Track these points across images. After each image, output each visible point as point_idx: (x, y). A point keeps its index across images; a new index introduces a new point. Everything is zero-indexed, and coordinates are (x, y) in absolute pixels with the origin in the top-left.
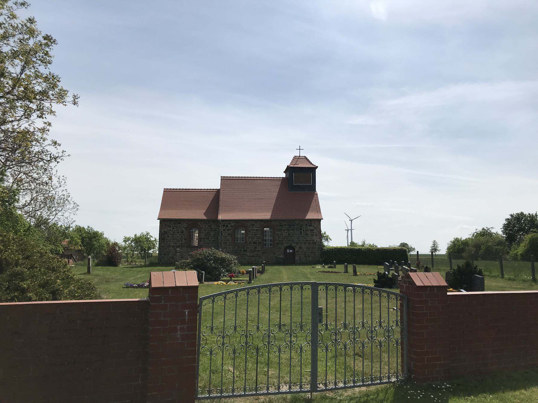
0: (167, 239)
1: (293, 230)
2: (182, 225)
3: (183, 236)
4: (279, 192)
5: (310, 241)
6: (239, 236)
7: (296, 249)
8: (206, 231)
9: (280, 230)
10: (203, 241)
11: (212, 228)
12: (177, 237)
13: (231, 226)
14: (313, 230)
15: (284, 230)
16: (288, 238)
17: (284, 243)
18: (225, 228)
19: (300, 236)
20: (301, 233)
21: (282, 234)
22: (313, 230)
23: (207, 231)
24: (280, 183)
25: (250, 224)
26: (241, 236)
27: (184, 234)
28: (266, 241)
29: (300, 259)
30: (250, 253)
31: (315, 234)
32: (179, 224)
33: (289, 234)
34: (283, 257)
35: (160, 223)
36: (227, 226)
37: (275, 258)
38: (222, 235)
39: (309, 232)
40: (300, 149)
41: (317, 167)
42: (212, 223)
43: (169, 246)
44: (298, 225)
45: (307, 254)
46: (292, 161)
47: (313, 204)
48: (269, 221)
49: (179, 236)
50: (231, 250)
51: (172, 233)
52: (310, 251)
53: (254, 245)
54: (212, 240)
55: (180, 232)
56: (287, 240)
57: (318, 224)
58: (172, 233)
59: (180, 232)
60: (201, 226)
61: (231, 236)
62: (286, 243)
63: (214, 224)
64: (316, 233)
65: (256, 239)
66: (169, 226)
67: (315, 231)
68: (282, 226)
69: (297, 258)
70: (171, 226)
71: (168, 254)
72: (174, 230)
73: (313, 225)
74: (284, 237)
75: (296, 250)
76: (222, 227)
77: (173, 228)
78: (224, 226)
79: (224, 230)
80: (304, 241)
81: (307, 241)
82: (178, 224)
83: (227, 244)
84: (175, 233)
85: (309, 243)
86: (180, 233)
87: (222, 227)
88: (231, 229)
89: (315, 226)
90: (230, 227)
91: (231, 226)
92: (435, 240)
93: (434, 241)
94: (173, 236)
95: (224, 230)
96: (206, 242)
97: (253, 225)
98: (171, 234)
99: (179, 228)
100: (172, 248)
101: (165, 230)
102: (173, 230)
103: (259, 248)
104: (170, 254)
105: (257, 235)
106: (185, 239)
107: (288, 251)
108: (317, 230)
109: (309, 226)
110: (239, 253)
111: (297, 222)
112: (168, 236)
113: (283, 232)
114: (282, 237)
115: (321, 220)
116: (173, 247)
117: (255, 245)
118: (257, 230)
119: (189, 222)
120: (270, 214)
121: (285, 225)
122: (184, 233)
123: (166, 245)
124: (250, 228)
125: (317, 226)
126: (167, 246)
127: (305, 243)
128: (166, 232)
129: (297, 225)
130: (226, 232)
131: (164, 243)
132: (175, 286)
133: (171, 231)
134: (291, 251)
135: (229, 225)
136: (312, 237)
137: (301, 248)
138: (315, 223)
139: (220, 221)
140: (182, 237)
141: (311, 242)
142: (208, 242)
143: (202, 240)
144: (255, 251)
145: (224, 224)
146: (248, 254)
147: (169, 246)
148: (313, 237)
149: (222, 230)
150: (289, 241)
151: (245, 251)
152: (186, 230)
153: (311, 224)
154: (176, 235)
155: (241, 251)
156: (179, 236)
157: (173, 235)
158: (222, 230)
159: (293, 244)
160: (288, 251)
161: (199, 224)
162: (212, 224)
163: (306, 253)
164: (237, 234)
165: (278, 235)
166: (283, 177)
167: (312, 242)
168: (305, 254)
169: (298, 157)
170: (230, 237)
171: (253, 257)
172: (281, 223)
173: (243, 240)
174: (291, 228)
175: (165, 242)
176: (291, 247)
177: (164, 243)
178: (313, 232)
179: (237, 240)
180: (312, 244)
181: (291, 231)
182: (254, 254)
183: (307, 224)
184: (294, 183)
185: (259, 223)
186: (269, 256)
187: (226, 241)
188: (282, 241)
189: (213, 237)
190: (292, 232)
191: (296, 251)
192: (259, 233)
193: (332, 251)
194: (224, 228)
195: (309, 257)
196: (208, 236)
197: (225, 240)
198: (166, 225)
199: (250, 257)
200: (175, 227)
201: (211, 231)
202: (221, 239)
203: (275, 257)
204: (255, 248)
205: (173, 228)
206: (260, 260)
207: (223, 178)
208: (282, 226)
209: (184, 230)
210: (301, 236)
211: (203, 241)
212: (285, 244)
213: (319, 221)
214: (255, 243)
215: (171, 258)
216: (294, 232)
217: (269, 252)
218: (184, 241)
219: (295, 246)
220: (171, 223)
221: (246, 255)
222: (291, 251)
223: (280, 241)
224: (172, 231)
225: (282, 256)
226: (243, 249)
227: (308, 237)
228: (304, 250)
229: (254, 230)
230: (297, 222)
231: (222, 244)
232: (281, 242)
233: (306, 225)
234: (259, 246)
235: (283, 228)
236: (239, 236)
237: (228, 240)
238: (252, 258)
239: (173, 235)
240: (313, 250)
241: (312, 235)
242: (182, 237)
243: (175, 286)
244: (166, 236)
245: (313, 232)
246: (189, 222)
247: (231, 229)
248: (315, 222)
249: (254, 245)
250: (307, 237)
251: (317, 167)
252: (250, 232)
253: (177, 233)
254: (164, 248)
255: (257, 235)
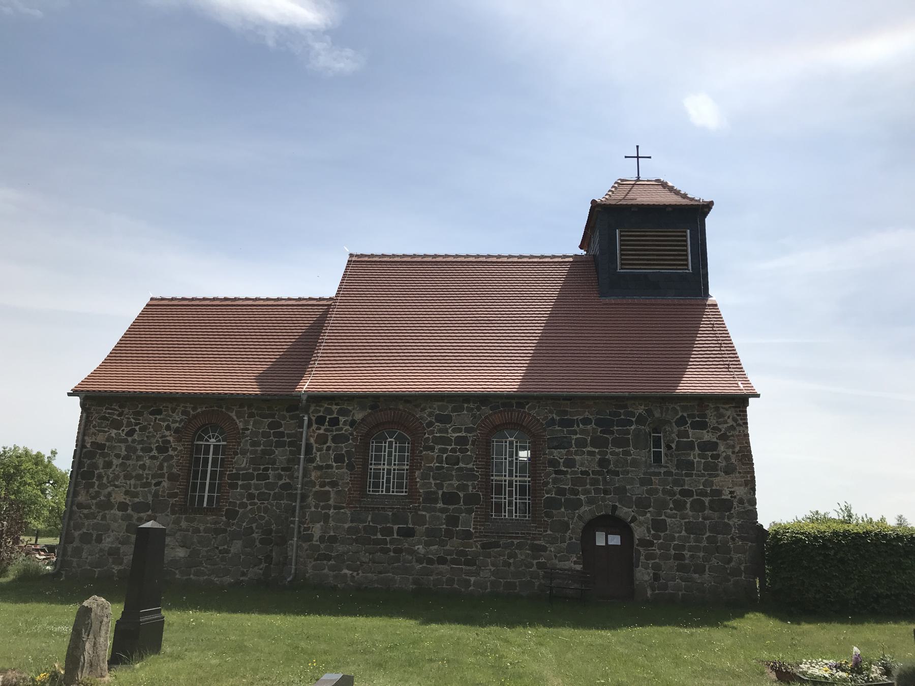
0: (100, 477)
1: (621, 442)
2: (164, 422)
3: (166, 464)
4: (560, 301)
5: (703, 493)
6: (386, 467)
7: (639, 532)
8: (254, 444)
9: (563, 444)
10: (243, 487)
11: (282, 435)
12: (143, 467)
13: (353, 423)
14: (714, 446)
15: (581, 443)
16: (600, 478)
17: (578, 504)
18: (326, 430)
19: (652, 470)
20: (657, 457)
21: (570, 463)
22: (714, 446)
23: (262, 447)
24: (565, 270)
25: (430, 415)
26: (393, 467)
27: (172, 457)
28: (499, 489)
29: (656, 577)
30: (427, 544)
31: (724, 464)
32: (153, 417)
33: (603, 463)
34: (579, 567)
35: (83, 405)
36: (334, 422)
37: (541, 573)
38: (312, 460)
39: (694, 456)
40: (638, 157)
41: (708, 206)
42: (285, 413)
43: (106, 505)
44: (641, 420)
45: (691, 556)
46: (613, 187)
47: (703, 340)
48: (514, 401)
49: (148, 462)
50: (346, 526)
51: (124, 453)
52: (705, 543)
53: (447, 510)
54: (281, 483)
55: (154, 446)
56: (597, 491)
57: (735, 420)
58: (124, 453)
59: (154, 446)
60: (241, 426)
61: (350, 467)
62: (590, 501)
63: (292, 418)
64: (727, 458)
65: (455, 483)
66: (117, 425)
67: (722, 448)
68: (570, 423)
69: (643, 575)
70: (125, 422)
71: (99, 540)
72: (134, 441)
73: (712, 420)
74: (582, 473)
75: (636, 536)
76: (315, 426)
77: (131, 433)
78: (320, 421)
79: (322, 440)
80: (675, 495)
81: (687, 493)
82: (152, 413)
83: (331, 502)
84: (136, 450)
85: (698, 506)
86: (154, 453)
87: (315, 426)
88: (352, 434)
89: (723, 427)
90: (348, 427)
91: (353, 423)
92: (902, 516)
93: (900, 517)
94: (128, 462)
95: (322, 440)
96: (252, 491)
97: (444, 419)
98: (118, 456)
99: (151, 430)
100: (117, 512)
101: (101, 439)
102: (130, 439)
103: (469, 522)
104: (108, 540)
105: (461, 465)
106: (173, 478)
107: (600, 540)
108: (733, 447)
109: (695, 426)
110: (377, 542)
111: (641, 410)
112: (108, 465)
113: (576, 453)
114: (575, 473)
115: (751, 400)
116: (123, 507)
117: (451, 507)
118: (462, 441)
119: (194, 409)
120: (520, 373)
121: (586, 421)
122: (171, 452)
123: (94, 501)
124: (432, 432)
125: (732, 428)
126: (96, 504)
127: (680, 506)
128: (101, 447)
129: (637, 422)
130: (329, 448)
131: (88, 492)
132: (604, 544)
133: (121, 441)
134: (615, 540)
135: (342, 419)
136: (710, 475)
137: (658, 525)
138: (721, 416)
139: (304, 398)
140: (161, 467)
141: (707, 500)
142: (263, 490)
143: (240, 483)
144: (449, 534)
145: (321, 414)
146: (420, 548)
147: (106, 505)
148: (717, 476)
149: (312, 440)
150: (606, 492)
151: (408, 533)
152: (180, 441)
153: (705, 416)
154: (139, 458)
155: (388, 532)
156: (148, 462)
157: (127, 457)
158: (312, 440)
159: (626, 509)
160: (600, 540)
161: (233, 415)
162: (284, 418)
163: (687, 554)
164: (378, 458)
165: (553, 463)
166: (576, 255)
167: (711, 502)
168: (679, 557)
169: (633, 183)
170: (345, 470)
171: (442, 561)
172: (565, 413)
173: (400, 486)
174: (612, 433)
175: (93, 487)
176: (612, 523)
177: (88, 492)
178: (712, 457)
179: (376, 485)
180: (711, 508)
181: (611, 448)
182: (448, 547)
183: (683, 417)
184: (622, 264)
185: (470, 410)
186: (511, 561)
187: (327, 488)
188: (576, 493)
189: (283, 469)
190: (617, 454)
191: (637, 542)
192: (469, 453)
193: (824, 546)
194: (322, 431)
195: (700, 570)
196: (262, 467)
197: (323, 485)
198: (104, 418)
199: (430, 561)
200: (137, 428)
201: (280, 444)
202: (306, 479)
203: (540, 566)
204: (453, 521)
205: (131, 433)
206: (473, 579)
207: (354, 259)
208: (570, 423)
209: (171, 439)
210: (657, 470)
211: (243, 487)
212: (585, 508)
213: (740, 402)
214: (450, 498)
215: (110, 554)
216: (627, 453)
217: (516, 541)
218: (165, 484)
219: (634, 519)
220: (126, 410)
221: (412, 552)
222: (615, 540)
223: (561, 492)
224: (126, 441)
225: (573, 564)
226: (396, 527)
227: (691, 475)
228: (673, 539)
229: (447, 441)
230: (641, 410)
231: (311, 500)
232: (568, 496)
233: (681, 422)
234: (469, 512)
235: (575, 433)
236: (386, 467)
237: (334, 484)
238: (436, 566)
239: (127, 457)
240: (720, 537)
241: (711, 468)
242: (161, 467)
243: (604, 544)
244: (100, 462)
245: (712, 457)
246: (194, 409)
247: (352, 434)
248: (722, 410)
249: (447, 510)
250: (687, 475)
251: (708, 206)
252: (432, 449)
253: (142, 449)
254: (86, 511)
255: (461, 465)
